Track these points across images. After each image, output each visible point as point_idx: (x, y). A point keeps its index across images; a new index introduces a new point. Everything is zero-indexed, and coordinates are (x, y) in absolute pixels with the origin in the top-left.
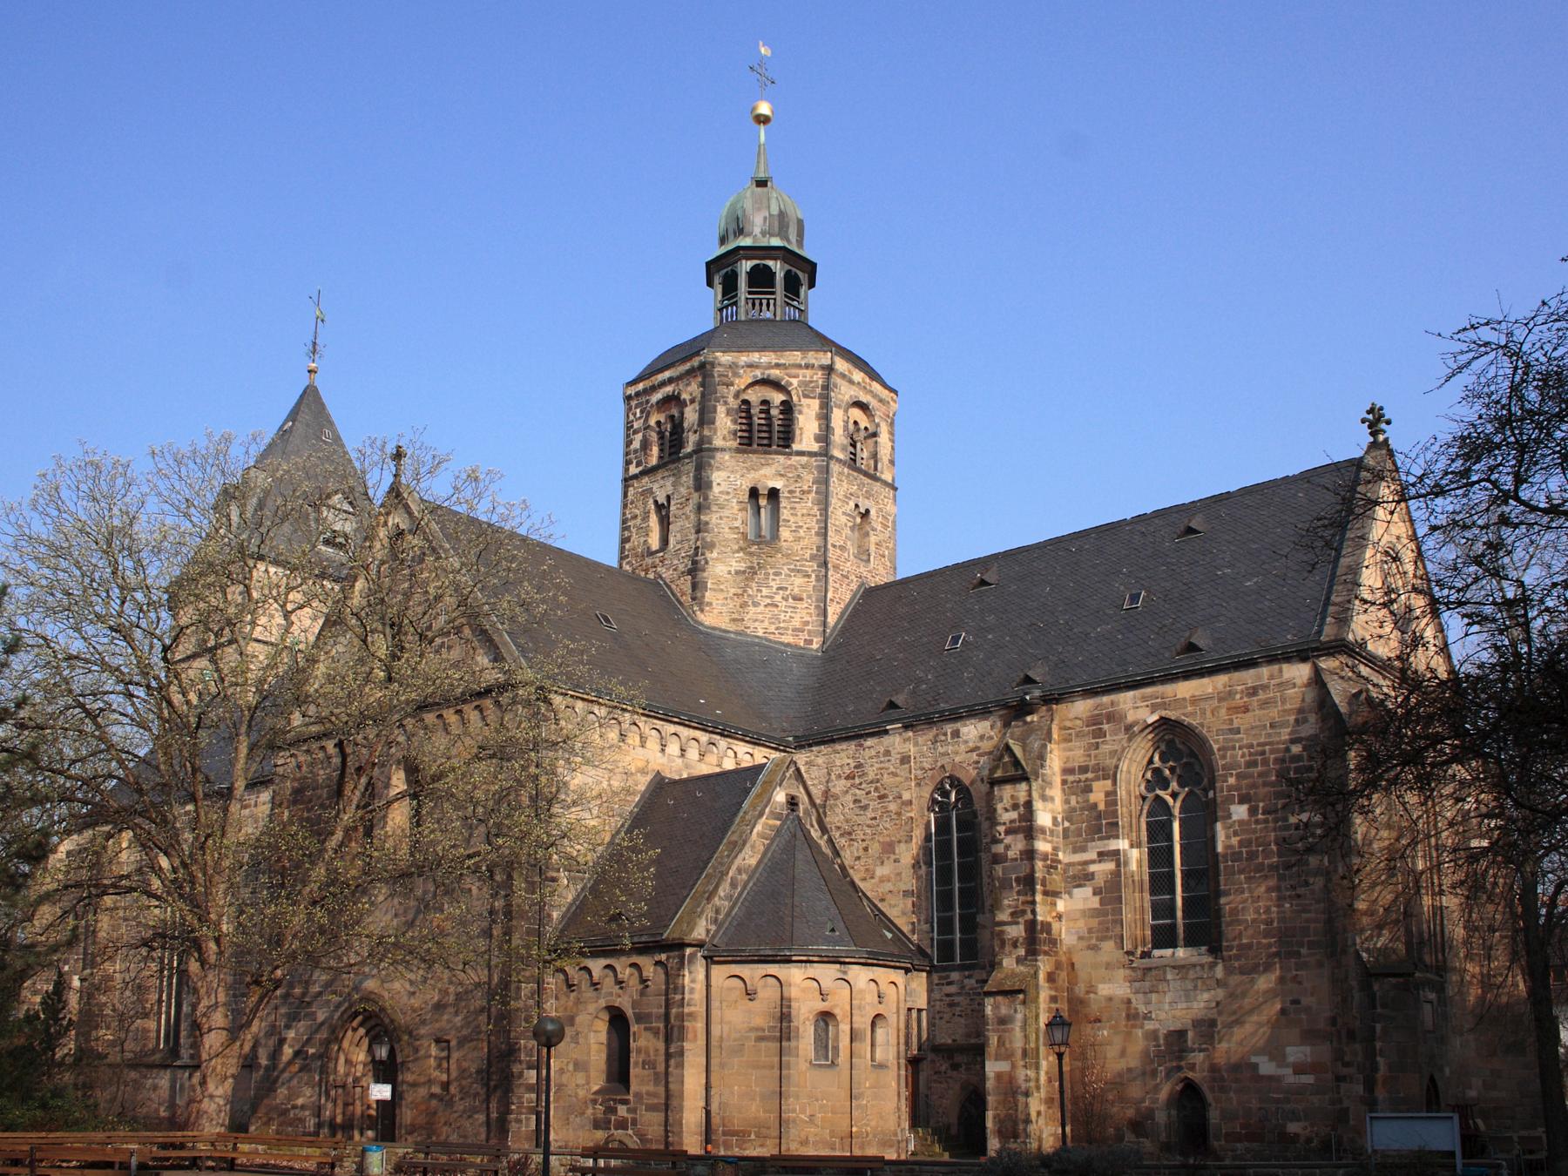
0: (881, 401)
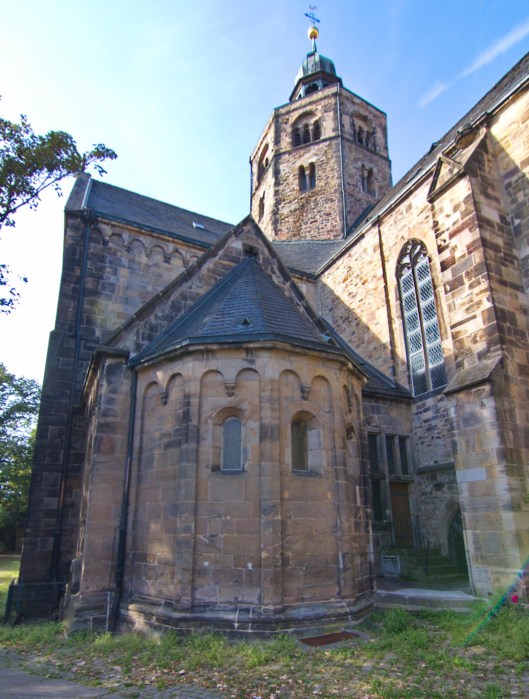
0: (375, 116)
